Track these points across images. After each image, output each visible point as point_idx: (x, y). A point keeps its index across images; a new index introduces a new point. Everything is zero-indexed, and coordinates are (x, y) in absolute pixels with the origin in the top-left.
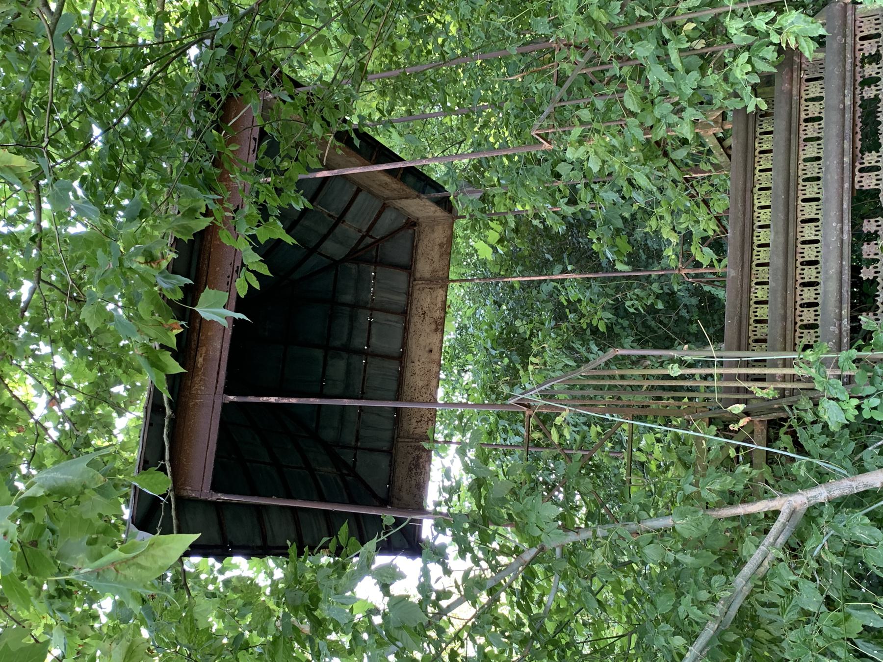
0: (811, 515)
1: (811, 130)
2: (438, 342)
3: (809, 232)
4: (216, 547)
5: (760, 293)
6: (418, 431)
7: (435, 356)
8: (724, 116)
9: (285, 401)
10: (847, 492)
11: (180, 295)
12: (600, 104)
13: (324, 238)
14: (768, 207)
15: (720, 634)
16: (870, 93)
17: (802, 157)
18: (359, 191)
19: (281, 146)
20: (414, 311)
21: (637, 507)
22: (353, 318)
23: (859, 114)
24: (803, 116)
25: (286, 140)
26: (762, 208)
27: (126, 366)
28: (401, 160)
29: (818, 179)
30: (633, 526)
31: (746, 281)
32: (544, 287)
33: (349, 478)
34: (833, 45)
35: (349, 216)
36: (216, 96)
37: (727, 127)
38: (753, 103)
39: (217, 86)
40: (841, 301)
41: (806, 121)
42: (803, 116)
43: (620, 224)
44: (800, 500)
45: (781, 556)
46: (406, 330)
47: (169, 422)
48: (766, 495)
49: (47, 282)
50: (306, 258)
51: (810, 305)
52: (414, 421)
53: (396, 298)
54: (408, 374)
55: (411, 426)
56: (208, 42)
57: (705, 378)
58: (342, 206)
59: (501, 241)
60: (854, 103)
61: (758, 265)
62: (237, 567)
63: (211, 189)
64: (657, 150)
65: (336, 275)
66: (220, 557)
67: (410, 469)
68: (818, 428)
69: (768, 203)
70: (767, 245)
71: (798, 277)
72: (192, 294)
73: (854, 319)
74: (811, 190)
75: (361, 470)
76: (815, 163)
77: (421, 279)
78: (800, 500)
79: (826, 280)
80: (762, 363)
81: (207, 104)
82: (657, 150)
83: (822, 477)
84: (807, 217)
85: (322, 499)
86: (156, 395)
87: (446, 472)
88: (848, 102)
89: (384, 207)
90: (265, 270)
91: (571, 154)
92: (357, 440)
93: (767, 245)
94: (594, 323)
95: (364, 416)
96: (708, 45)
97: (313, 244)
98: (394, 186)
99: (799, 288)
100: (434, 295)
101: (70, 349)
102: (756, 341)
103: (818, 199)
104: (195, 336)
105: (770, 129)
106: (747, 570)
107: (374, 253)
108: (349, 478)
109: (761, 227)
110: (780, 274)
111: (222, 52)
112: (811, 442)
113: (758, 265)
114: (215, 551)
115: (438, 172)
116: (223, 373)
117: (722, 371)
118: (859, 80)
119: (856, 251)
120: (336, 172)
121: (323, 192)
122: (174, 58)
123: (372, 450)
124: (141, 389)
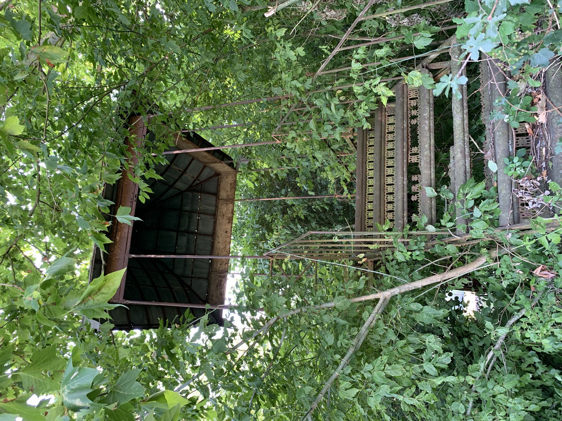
0: (392, 300)
1: (390, 137)
2: (230, 228)
3: (390, 180)
4: (126, 325)
5: (370, 206)
6: (220, 269)
7: (229, 234)
8: (354, 130)
9: (159, 256)
11: (107, 211)
12: (301, 124)
13: (177, 181)
14: (372, 169)
15: (355, 353)
16: (414, 122)
17: (387, 148)
18: (193, 159)
19: (156, 136)
20: (219, 214)
21: (319, 298)
22: (190, 218)
23: (409, 131)
24: (387, 131)
25: (159, 133)
26: (370, 170)
27: (82, 241)
28: (213, 146)
29: (393, 158)
30: (318, 306)
31: (364, 201)
33: (188, 292)
34: (398, 101)
35: (188, 171)
36: (126, 112)
37: (355, 135)
38: (367, 126)
39: (126, 108)
40: (403, 210)
41: (388, 133)
42: (387, 131)
43: (309, 175)
44: (388, 294)
45: (380, 317)
46: (215, 223)
47: (104, 268)
48: (373, 292)
49: (42, 202)
50: (168, 190)
51: (390, 211)
52: (219, 264)
53: (211, 208)
54: (216, 243)
55: (218, 266)
56: (122, 87)
57: (348, 243)
58: (185, 166)
59: (257, 180)
60: (408, 126)
61: (369, 194)
62: (135, 333)
63: (123, 154)
64: (326, 144)
65: (182, 198)
66: (128, 330)
67: (217, 286)
68: (394, 262)
69: (373, 152)
70: (372, 186)
71: (386, 199)
72: (114, 209)
73: (409, 217)
74: (390, 162)
75: (194, 287)
76: (392, 151)
77: (222, 199)
78: (388, 294)
79: (397, 201)
80: (371, 236)
81: (121, 116)
83: (395, 284)
84: (389, 174)
85: (176, 302)
86: (98, 249)
87: (233, 285)
88: (405, 126)
89: (205, 167)
90: (150, 191)
91: (288, 145)
92: (192, 273)
93: (372, 186)
94: (299, 215)
95: (195, 262)
96: (347, 99)
97: (171, 183)
98: (209, 157)
99: (386, 213)
100: (228, 207)
101: (54, 233)
102: (368, 227)
103: (393, 167)
104: (115, 227)
105: (373, 136)
106: (366, 325)
107: (200, 188)
108: (188, 292)
109: (369, 178)
110: (378, 198)
111: (130, 92)
112: (392, 268)
113: (369, 194)
114: (125, 327)
116: (129, 244)
117: (355, 240)
118: (410, 116)
119: (409, 189)
120: (183, 151)
121: (176, 160)
122: (106, 94)
123: (199, 278)
124: (89, 251)
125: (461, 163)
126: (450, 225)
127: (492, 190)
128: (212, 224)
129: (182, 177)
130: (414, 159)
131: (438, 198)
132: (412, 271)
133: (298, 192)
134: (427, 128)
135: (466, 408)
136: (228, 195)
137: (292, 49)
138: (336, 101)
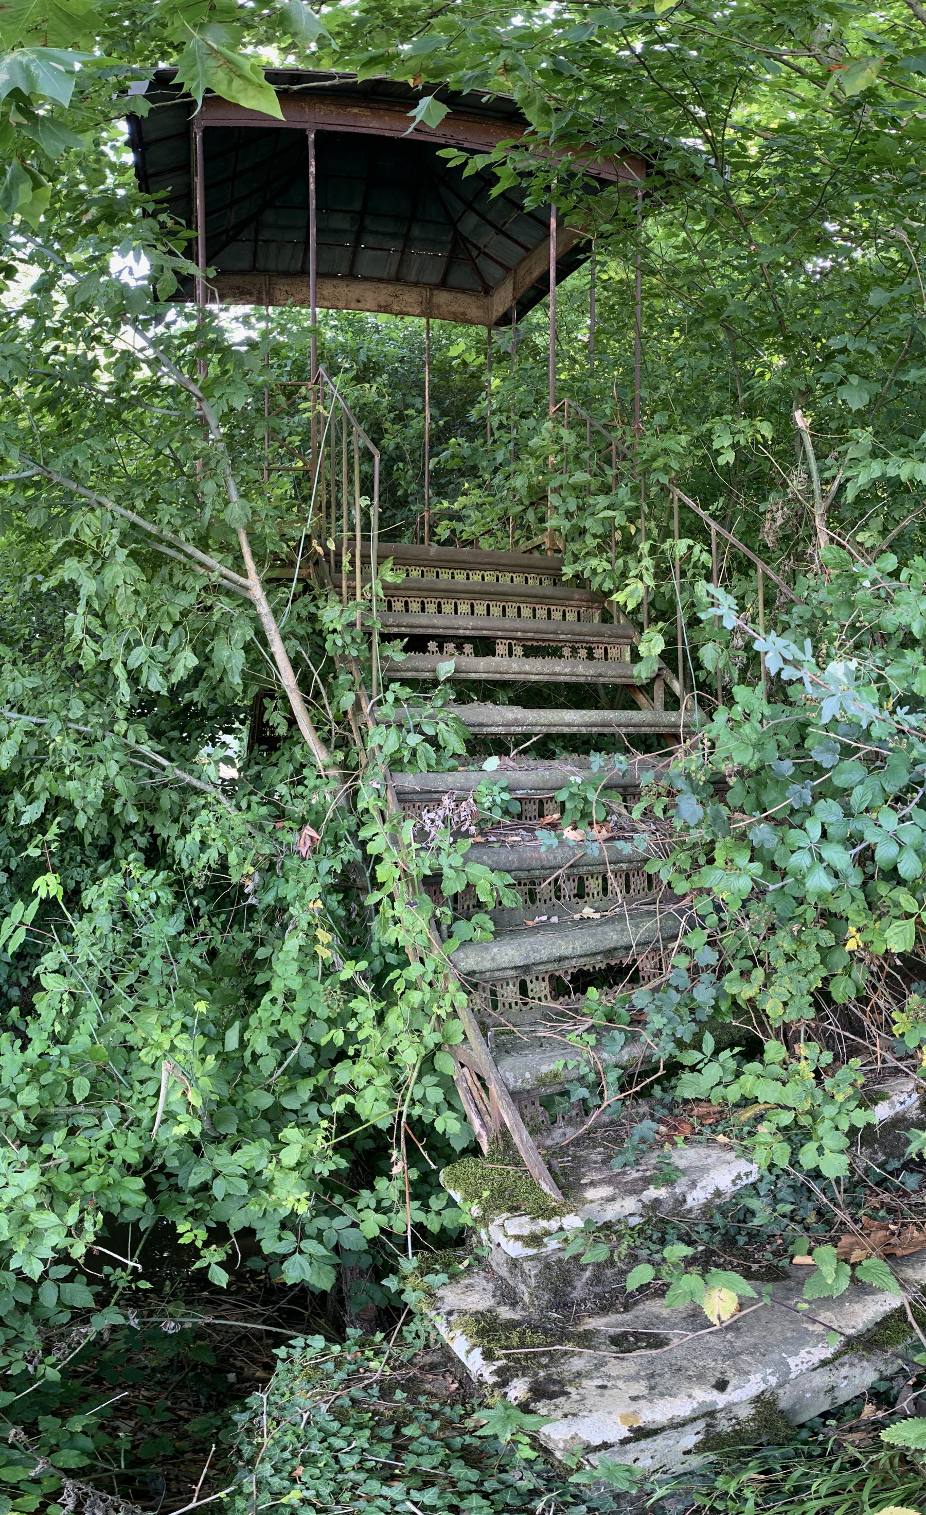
1: (541, 613)
3: (464, 608)
8: (559, 551)
10: (267, 627)
13: (482, 216)
16: (566, 652)
18: (527, 250)
22: (394, 236)
32: (419, 400)
33: (224, 237)
35: (502, 238)
36: (655, 155)
38: (568, 571)
46: (380, 280)
53: (414, 272)
54: (335, 282)
64: (538, 497)
82: (538, 497)
83: (275, 612)
89: (507, 269)
92: (265, 241)
97: (476, 206)
108: (224, 237)
115: (536, 316)
116: (340, 129)
123: (255, 254)
125: (498, 719)
126: (390, 696)
127: (453, 762)
128: (378, 275)
129: (488, 227)
130: (501, 648)
131: (435, 683)
132: (301, 639)
133: (440, 437)
134: (558, 669)
135: (77, 721)
136: (439, 306)
137: (734, 446)
138: (620, 519)
